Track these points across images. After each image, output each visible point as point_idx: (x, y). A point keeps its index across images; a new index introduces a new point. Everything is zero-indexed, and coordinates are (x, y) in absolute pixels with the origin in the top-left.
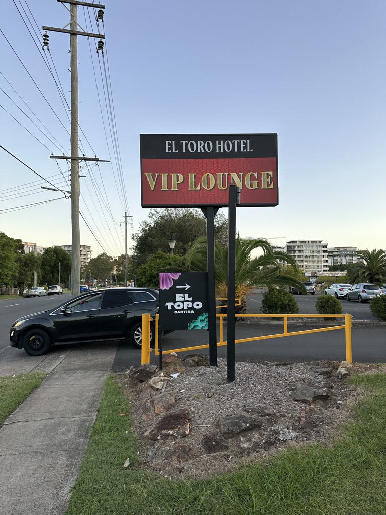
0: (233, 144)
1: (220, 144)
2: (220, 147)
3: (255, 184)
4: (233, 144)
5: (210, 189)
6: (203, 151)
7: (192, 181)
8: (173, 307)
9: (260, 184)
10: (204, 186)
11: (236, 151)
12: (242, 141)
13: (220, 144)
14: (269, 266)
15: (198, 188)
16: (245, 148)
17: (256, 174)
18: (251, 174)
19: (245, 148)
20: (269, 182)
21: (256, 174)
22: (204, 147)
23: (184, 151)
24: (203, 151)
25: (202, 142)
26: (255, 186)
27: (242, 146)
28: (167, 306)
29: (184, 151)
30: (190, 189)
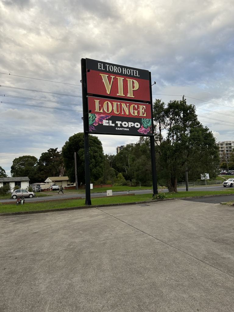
0: (131, 71)
1: (124, 70)
2: (124, 72)
3: (136, 112)
4: (131, 71)
5: (109, 112)
6: (117, 72)
7: (97, 105)
8: (121, 124)
9: (138, 113)
10: (106, 110)
11: (132, 75)
12: (134, 71)
13: (124, 70)
14: (138, 222)
15: (101, 111)
16: (136, 74)
17: (136, 106)
18: (134, 106)
19: (136, 74)
20: (144, 112)
21: (136, 106)
22: (117, 70)
23: (108, 70)
24: (117, 72)
25: (116, 67)
26: (136, 114)
27: (135, 73)
28: (117, 124)
29: (108, 70)
30: (96, 111)
